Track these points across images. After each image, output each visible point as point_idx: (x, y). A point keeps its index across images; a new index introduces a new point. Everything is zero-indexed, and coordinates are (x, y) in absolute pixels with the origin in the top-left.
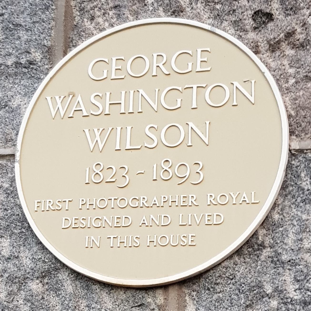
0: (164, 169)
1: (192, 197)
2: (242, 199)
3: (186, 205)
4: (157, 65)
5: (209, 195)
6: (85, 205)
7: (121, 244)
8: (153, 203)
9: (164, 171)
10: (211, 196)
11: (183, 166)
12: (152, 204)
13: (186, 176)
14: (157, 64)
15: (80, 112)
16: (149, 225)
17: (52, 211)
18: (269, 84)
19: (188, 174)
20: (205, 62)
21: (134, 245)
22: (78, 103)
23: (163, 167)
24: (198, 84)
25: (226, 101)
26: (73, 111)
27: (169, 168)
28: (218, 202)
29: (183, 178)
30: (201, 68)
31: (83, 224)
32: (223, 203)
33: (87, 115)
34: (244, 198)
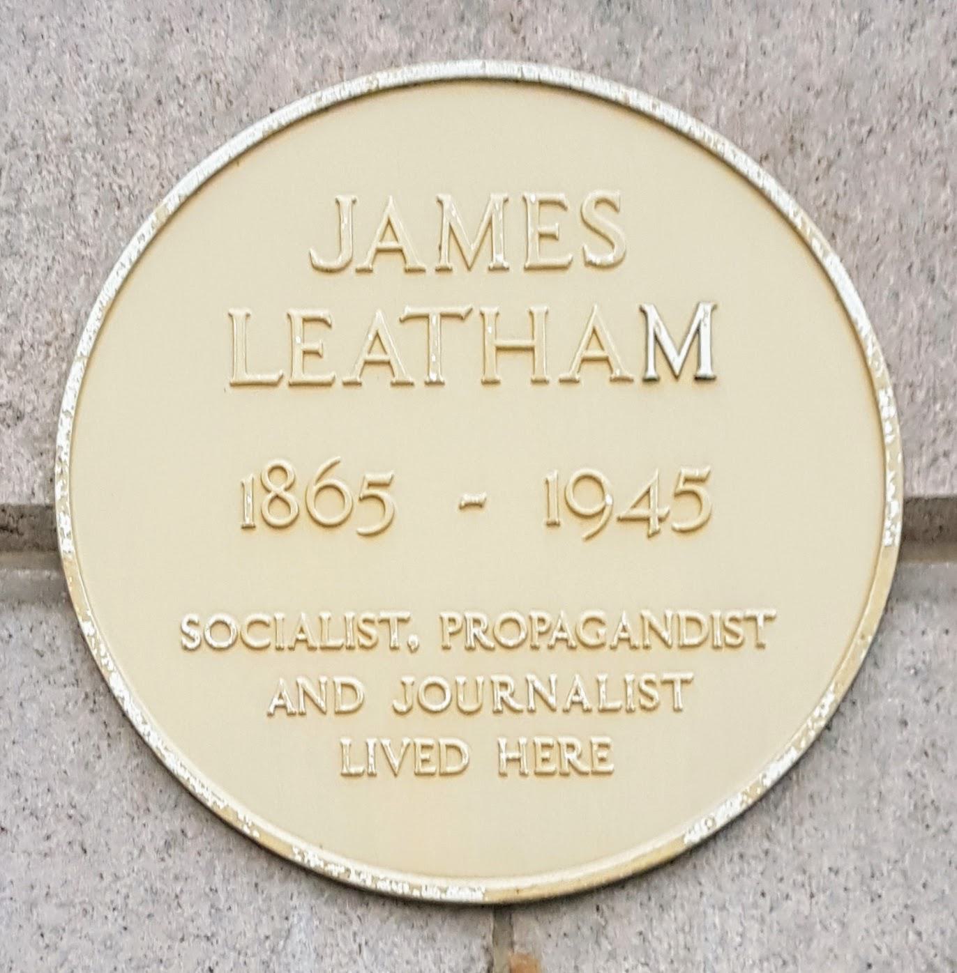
11: (326, 493)
20: (321, 326)
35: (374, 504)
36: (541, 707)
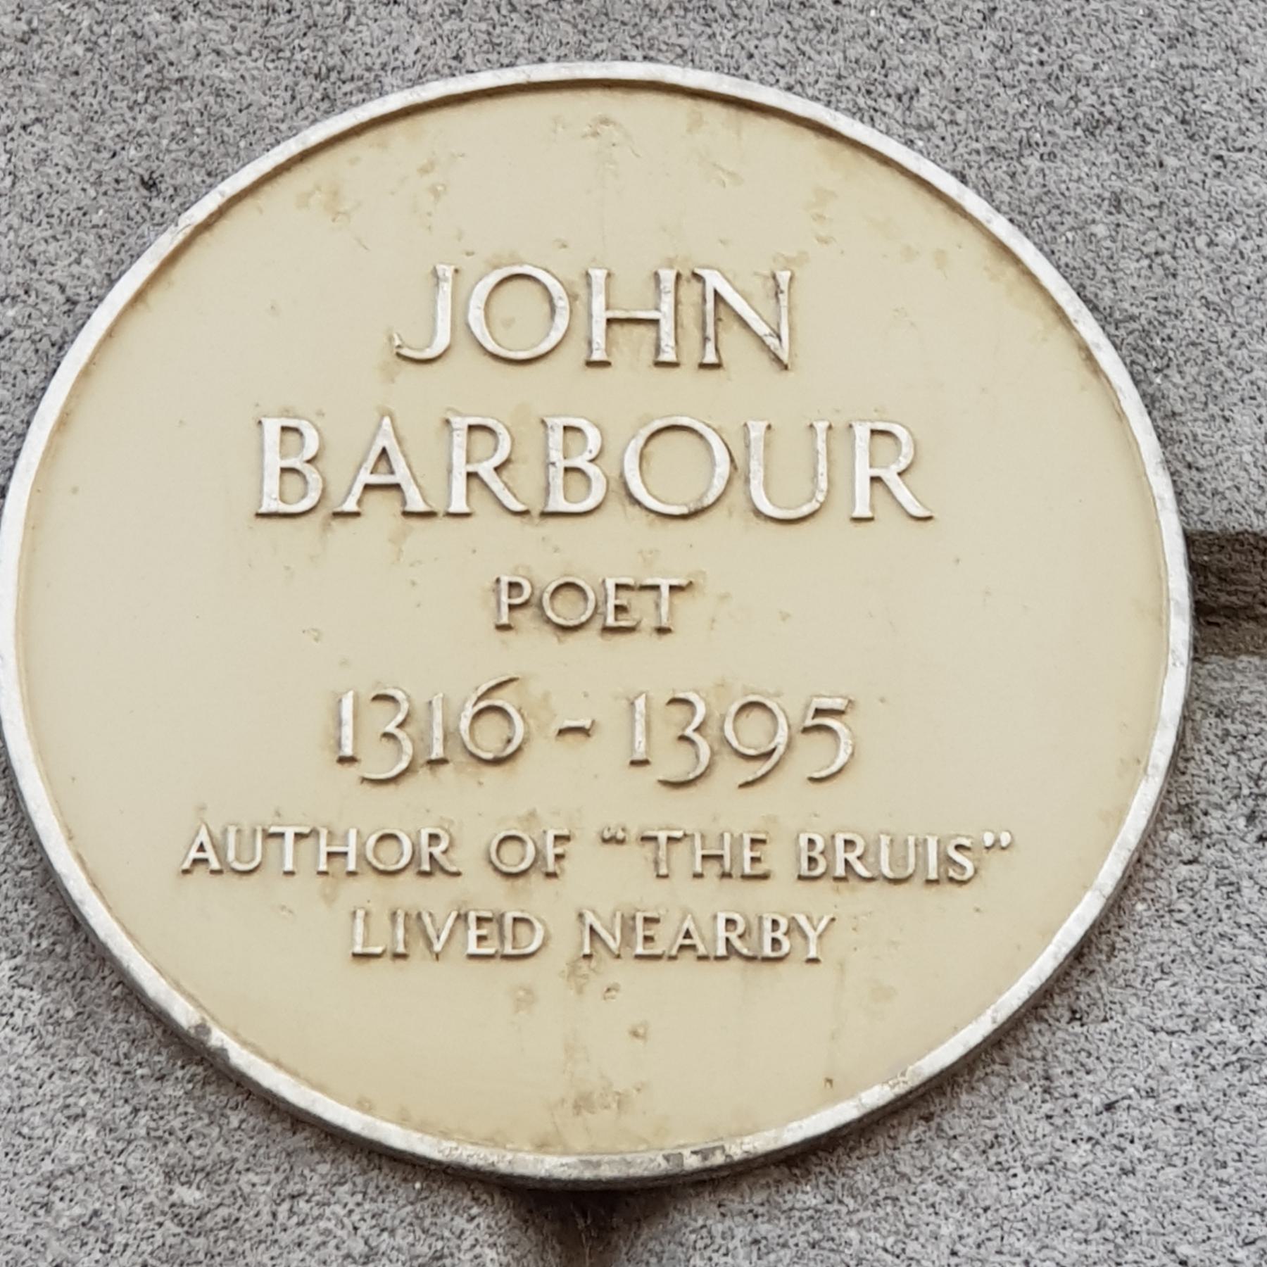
2: (194, 854)
7: (337, 862)
13: (774, 750)
15: (393, 494)
26: (358, 489)
35: (818, 738)
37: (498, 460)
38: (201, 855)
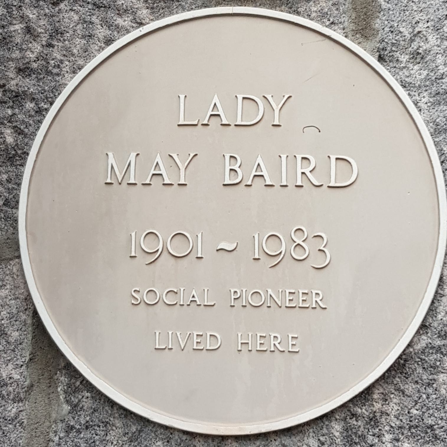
0: (295, 242)
1: (317, 294)
3: (307, 306)
4: (303, 171)
5: (232, 291)
6: (240, 299)
7: (244, 346)
8: (191, 299)
9: (296, 246)
10: (317, 294)
12: (190, 301)
14: (301, 168)
16: (202, 304)
17: (278, 352)
18: (432, 167)
19: (160, 247)
21: (133, 302)
22: (214, 106)
23: (295, 239)
24: (337, 155)
25: (351, 183)
27: (304, 241)
28: (143, 298)
29: (156, 253)
30: (230, 180)
31: (137, 299)
32: (253, 304)
33: (227, 123)
34: (193, 297)
36: (273, 305)
37: (311, 168)
38: (193, 299)
